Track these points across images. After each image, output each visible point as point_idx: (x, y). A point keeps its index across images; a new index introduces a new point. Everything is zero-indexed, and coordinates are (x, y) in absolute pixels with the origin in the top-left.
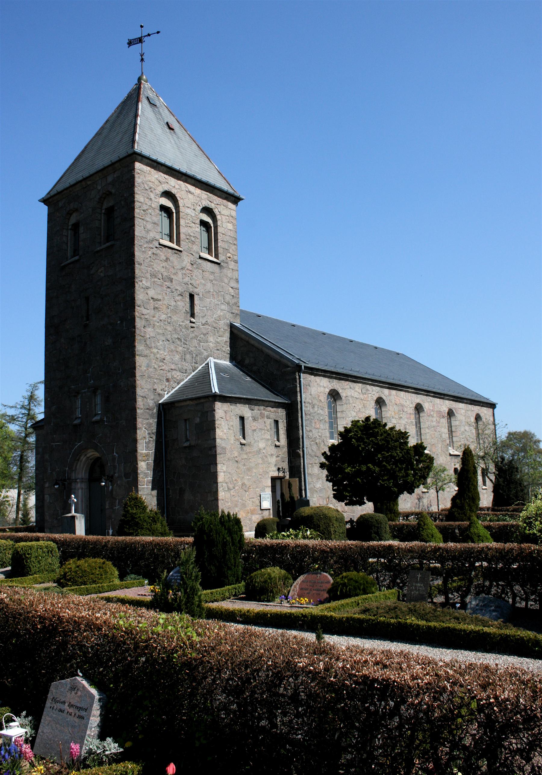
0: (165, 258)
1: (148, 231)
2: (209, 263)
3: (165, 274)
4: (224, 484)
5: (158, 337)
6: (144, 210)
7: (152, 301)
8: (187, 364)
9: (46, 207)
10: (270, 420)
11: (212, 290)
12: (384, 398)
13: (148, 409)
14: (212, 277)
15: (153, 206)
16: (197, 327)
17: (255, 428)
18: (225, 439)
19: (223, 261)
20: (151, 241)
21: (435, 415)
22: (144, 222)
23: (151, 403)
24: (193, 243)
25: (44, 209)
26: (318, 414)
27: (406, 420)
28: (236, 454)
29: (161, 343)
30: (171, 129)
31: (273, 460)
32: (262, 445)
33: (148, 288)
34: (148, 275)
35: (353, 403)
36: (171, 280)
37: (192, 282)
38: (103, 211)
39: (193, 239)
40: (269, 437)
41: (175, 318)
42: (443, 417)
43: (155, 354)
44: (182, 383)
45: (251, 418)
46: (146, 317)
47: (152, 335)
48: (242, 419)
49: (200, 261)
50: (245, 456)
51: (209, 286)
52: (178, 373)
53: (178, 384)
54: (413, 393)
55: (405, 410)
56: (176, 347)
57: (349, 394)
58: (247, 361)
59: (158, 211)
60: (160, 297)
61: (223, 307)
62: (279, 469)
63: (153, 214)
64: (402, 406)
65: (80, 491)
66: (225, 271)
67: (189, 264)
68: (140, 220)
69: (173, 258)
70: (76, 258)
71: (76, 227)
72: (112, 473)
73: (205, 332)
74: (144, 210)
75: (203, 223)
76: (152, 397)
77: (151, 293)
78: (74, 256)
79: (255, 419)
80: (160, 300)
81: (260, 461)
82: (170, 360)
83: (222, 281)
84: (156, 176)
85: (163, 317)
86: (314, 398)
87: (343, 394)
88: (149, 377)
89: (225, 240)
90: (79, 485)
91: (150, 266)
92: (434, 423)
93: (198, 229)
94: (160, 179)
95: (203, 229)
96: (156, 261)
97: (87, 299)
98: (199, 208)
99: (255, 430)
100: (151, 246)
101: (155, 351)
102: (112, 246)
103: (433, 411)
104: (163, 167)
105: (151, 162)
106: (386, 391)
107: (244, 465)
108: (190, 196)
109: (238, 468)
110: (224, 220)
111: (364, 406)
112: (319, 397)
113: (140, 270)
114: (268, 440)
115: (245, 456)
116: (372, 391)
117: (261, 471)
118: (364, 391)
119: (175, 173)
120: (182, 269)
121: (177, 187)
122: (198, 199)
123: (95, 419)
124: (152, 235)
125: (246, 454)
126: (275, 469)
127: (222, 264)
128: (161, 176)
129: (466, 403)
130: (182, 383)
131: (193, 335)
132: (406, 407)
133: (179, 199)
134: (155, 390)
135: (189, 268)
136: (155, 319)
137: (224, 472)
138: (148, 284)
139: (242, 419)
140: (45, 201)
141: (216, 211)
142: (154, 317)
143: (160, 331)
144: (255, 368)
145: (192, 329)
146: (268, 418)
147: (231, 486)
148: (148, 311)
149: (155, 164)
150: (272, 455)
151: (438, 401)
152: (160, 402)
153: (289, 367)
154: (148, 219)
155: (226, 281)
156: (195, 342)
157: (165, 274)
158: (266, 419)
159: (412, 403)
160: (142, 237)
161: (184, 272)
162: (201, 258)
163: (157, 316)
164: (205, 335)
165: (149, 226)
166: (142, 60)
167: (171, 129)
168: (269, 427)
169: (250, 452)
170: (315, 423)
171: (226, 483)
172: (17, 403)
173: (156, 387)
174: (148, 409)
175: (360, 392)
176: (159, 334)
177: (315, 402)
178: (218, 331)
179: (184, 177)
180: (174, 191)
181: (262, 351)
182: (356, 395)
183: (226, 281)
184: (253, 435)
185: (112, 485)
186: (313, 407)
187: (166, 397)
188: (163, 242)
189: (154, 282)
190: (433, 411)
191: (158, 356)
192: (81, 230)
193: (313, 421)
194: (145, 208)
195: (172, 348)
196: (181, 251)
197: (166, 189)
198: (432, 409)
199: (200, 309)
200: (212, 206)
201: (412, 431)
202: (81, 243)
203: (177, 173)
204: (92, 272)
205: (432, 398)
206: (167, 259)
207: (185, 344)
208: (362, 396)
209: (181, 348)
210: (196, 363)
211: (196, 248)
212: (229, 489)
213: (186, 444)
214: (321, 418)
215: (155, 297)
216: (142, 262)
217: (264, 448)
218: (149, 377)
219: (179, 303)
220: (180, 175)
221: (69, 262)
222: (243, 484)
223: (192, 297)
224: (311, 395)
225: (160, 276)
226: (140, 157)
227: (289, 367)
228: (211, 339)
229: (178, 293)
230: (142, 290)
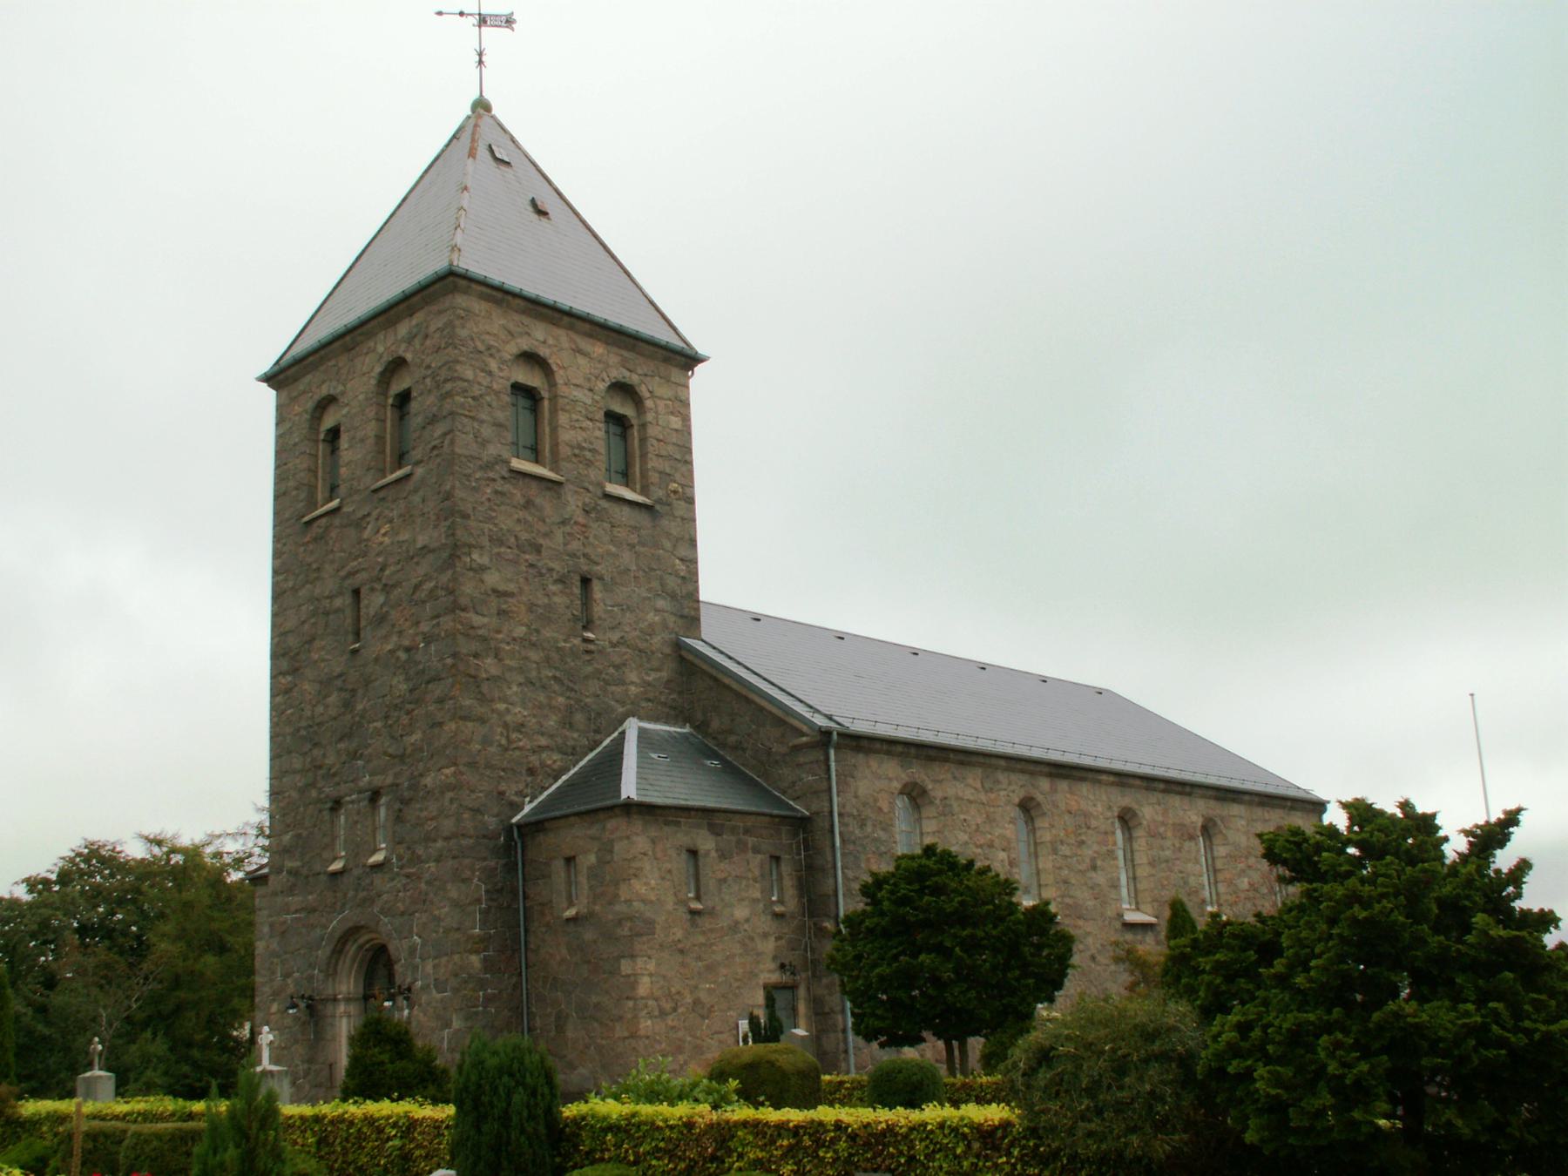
0: (522, 501)
1: (484, 443)
2: (626, 509)
3: (524, 536)
4: (650, 1002)
5: (508, 675)
6: (474, 398)
7: (493, 597)
8: (576, 735)
9: (274, 392)
10: (759, 857)
11: (634, 568)
12: (1040, 798)
13: (484, 836)
14: (634, 539)
15: (495, 386)
16: (600, 652)
17: (723, 876)
18: (651, 902)
19: (659, 501)
20: (488, 466)
21: (1169, 834)
22: (476, 425)
23: (492, 822)
24: (589, 464)
25: (269, 395)
26: (875, 840)
27: (1096, 847)
28: (679, 935)
29: (515, 688)
30: (542, 213)
31: (769, 946)
32: (741, 913)
33: (483, 569)
34: (485, 542)
35: (962, 812)
36: (538, 549)
37: (588, 550)
38: (390, 401)
39: (588, 455)
40: (758, 895)
41: (548, 633)
42: (1192, 838)
43: (500, 714)
44: (564, 778)
45: (713, 854)
46: (480, 632)
47: (494, 671)
48: (693, 853)
49: (604, 504)
50: (701, 939)
51: (627, 558)
52: (556, 756)
53: (556, 779)
54: (1113, 784)
55: (1094, 823)
56: (550, 698)
57: (951, 792)
58: (715, 724)
59: (507, 399)
60: (512, 587)
61: (661, 603)
62: (782, 966)
63: (494, 404)
64: (1086, 815)
65: (344, 1021)
66: (665, 522)
67: (579, 512)
68: (465, 420)
69: (544, 501)
70: (335, 503)
71: (334, 433)
72: (409, 980)
73: (617, 660)
74: (474, 398)
75: (612, 418)
76: (496, 810)
77: (492, 579)
78: (331, 499)
79: (723, 855)
80: (511, 595)
81: (737, 949)
82: (536, 727)
83: (657, 546)
84: (502, 322)
85: (520, 631)
86: (865, 804)
87: (937, 793)
88: (488, 766)
89: (663, 453)
90: (342, 1008)
91: (490, 519)
92: (1168, 853)
93: (598, 433)
94: (511, 326)
95: (612, 428)
96: (503, 508)
97: (356, 593)
98: (602, 386)
99: (724, 880)
100: (491, 475)
101: (502, 706)
102: (408, 477)
103: (1163, 824)
104: (518, 301)
105: (488, 291)
106: (1045, 784)
107: (699, 958)
108: (581, 360)
109: (683, 965)
110: (661, 409)
111: (990, 819)
112: (876, 800)
113: (466, 528)
114: (755, 901)
115: (701, 939)
116: (1010, 784)
117: (740, 971)
118: (987, 786)
119: (545, 311)
120: (564, 523)
121: (551, 341)
122: (600, 366)
123: (372, 860)
124: (492, 450)
125: (703, 933)
126: (772, 966)
127: (658, 507)
128: (514, 321)
129: (1250, 803)
130: (564, 778)
131: (589, 669)
132: (1097, 818)
133: (554, 368)
134: (502, 794)
135: (581, 520)
136: (500, 636)
137: (651, 975)
138: (485, 560)
139: (693, 853)
140: (271, 379)
141: (643, 391)
142: (499, 632)
143: (512, 663)
144: (732, 739)
145: (587, 657)
146: (756, 850)
147: (668, 1006)
148: (486, 620)
149: (499, 295)
150: (765, 936)
151: (1176, 801)
152: (514, 820)
153: (803, 734)
154: (483, 416)
155: (668, 545)
156: (594, 686)
157: (524, 536)
158: (750, 854)
159: (1110, 808)
160: (471, 458)
161: (568, 529)
162: (609, 497)
163: (505, 629)
164: (617, 667)
165: (487, 431)
166: (481, 62)
167: (542, 213)
168: (757, 872)
169: (711, 930)
170: (868, 860)
171: (656, 1000)
172: (247, 824)
173: (503, 787)
174: (484, 836)
175: (979, 785)
176: (511, 669)
177: (868, 812)
178: (649, 660)
179: (566, 319)
180: (543, 352)
181: (748, 701)
182: (969, 794)
183: (668, 545)
184: (720, 890)
185: (411, 1007)
186: (862, 825)
187: (527, 809)
188: (517, 464)
189: (498, 554)
190: (1163, 824)
191: (508, 718)
192: (344, 442)
193: (863, 857)
194: (477, 393)
195: (542, 698)
196: (559, 484)
197: (525, 348)
198: (1160, 818)
199: (607, 612)
200: (634, 379)
201: (1022, 875)
202: (343, 470)
203: (550, 312)
204: (366, 535)
205: (1160, 795)
206: (528, 504)
207: (572, 690)
208: (983, 797)
209: (561, 699)
210: (597, 731)
211: (595, 474)
212: (663, 1014)
213: (570, 913)
214: (883, 849)
215: (502, 587)
216: (470, 511)
217: (747, 920)
218: (488, 766)
219: (556, 599)
220: (557, 315)
221: (317, 513)
222: (697, 1002)
223: (586, 581)
224: (856, 797)
225: (512, 540)
226: (463, 283)
227: (803, 734)
228: (633, 676)
229: (555, 576)
230: (471, 574)
